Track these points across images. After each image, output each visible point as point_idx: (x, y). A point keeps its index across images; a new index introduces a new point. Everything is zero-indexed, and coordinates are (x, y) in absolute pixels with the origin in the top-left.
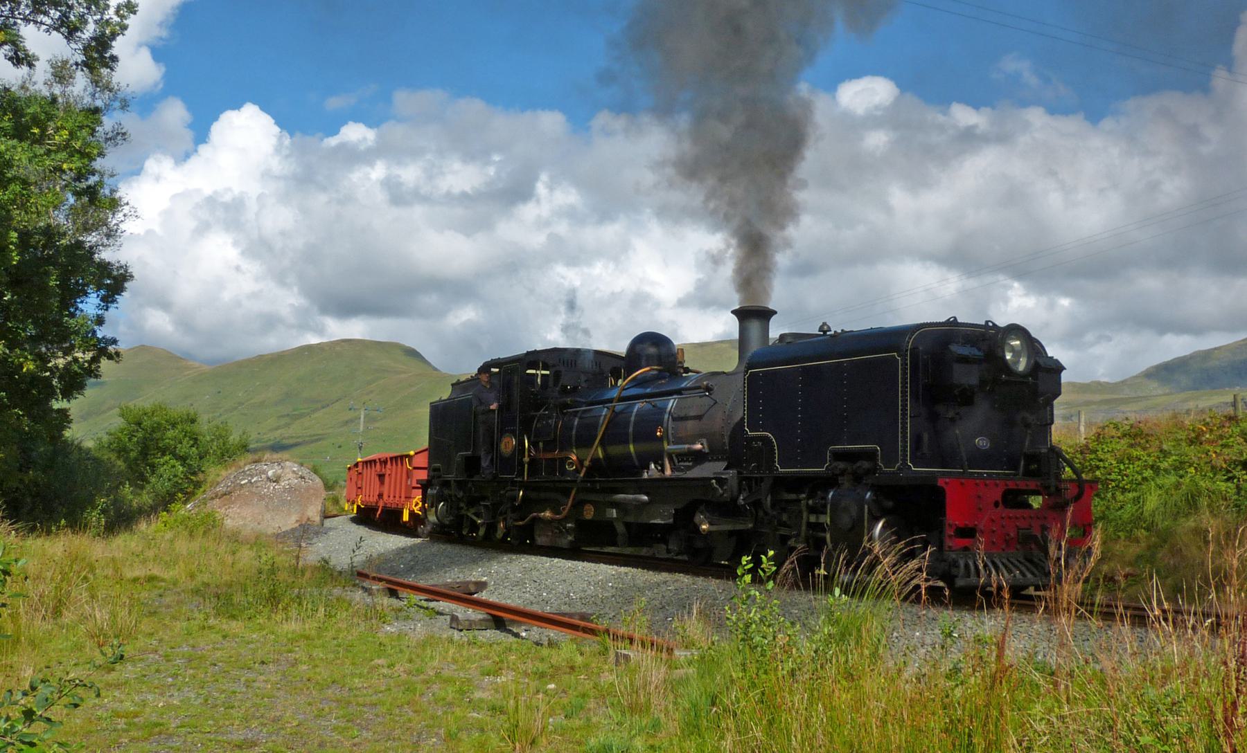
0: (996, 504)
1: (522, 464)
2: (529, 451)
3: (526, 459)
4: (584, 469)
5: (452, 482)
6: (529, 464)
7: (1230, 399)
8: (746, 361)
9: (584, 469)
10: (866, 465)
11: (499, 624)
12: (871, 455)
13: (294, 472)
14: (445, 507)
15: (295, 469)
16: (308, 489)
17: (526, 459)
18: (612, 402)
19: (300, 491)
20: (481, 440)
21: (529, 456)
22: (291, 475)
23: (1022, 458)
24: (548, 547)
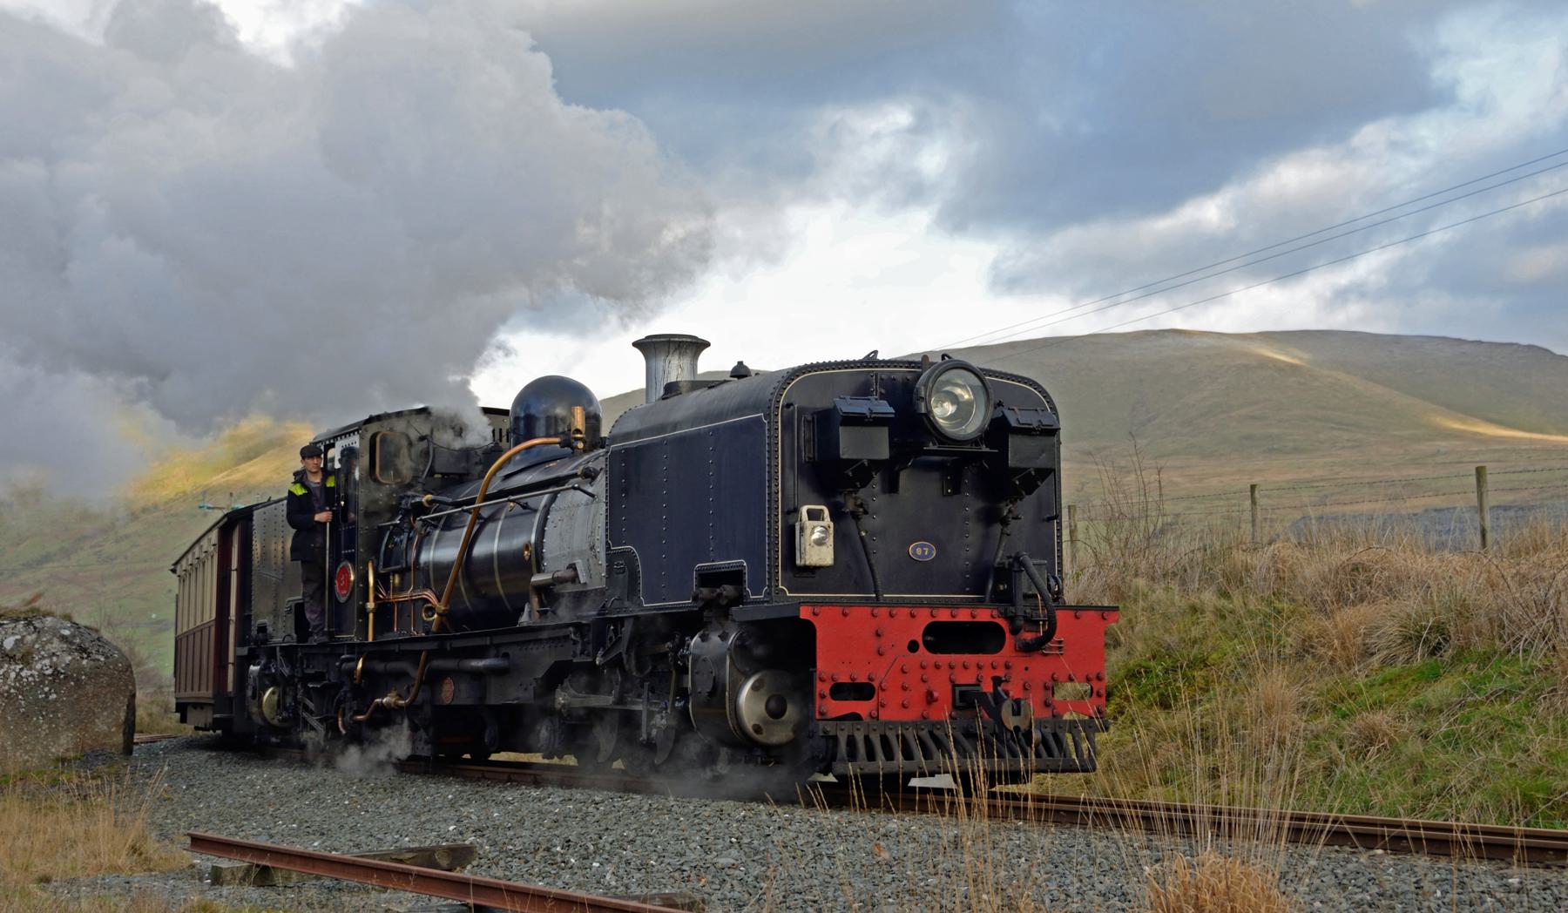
0: (913, 646)
1: (363, 613)
2: (376, 589)
3: (371, 605)
4: (371, 616)
5: (278, 649)
6: (377, 612)
7: (1246, 483)
8: (992, 402)
9: (371, 616)
10: (728, 590)
11: (263, 877)
12: (735, 577)
13: (64, 638)
14: (276, 698)
15: (67, 632)
16: (95, 674)
17: (371, 605)
18: (474, 503)
19: (78, 680)
20: (1038, 576)
21: (376, 598)
22: (56, 645)
23: (992, 576)
24: (134, 721)
